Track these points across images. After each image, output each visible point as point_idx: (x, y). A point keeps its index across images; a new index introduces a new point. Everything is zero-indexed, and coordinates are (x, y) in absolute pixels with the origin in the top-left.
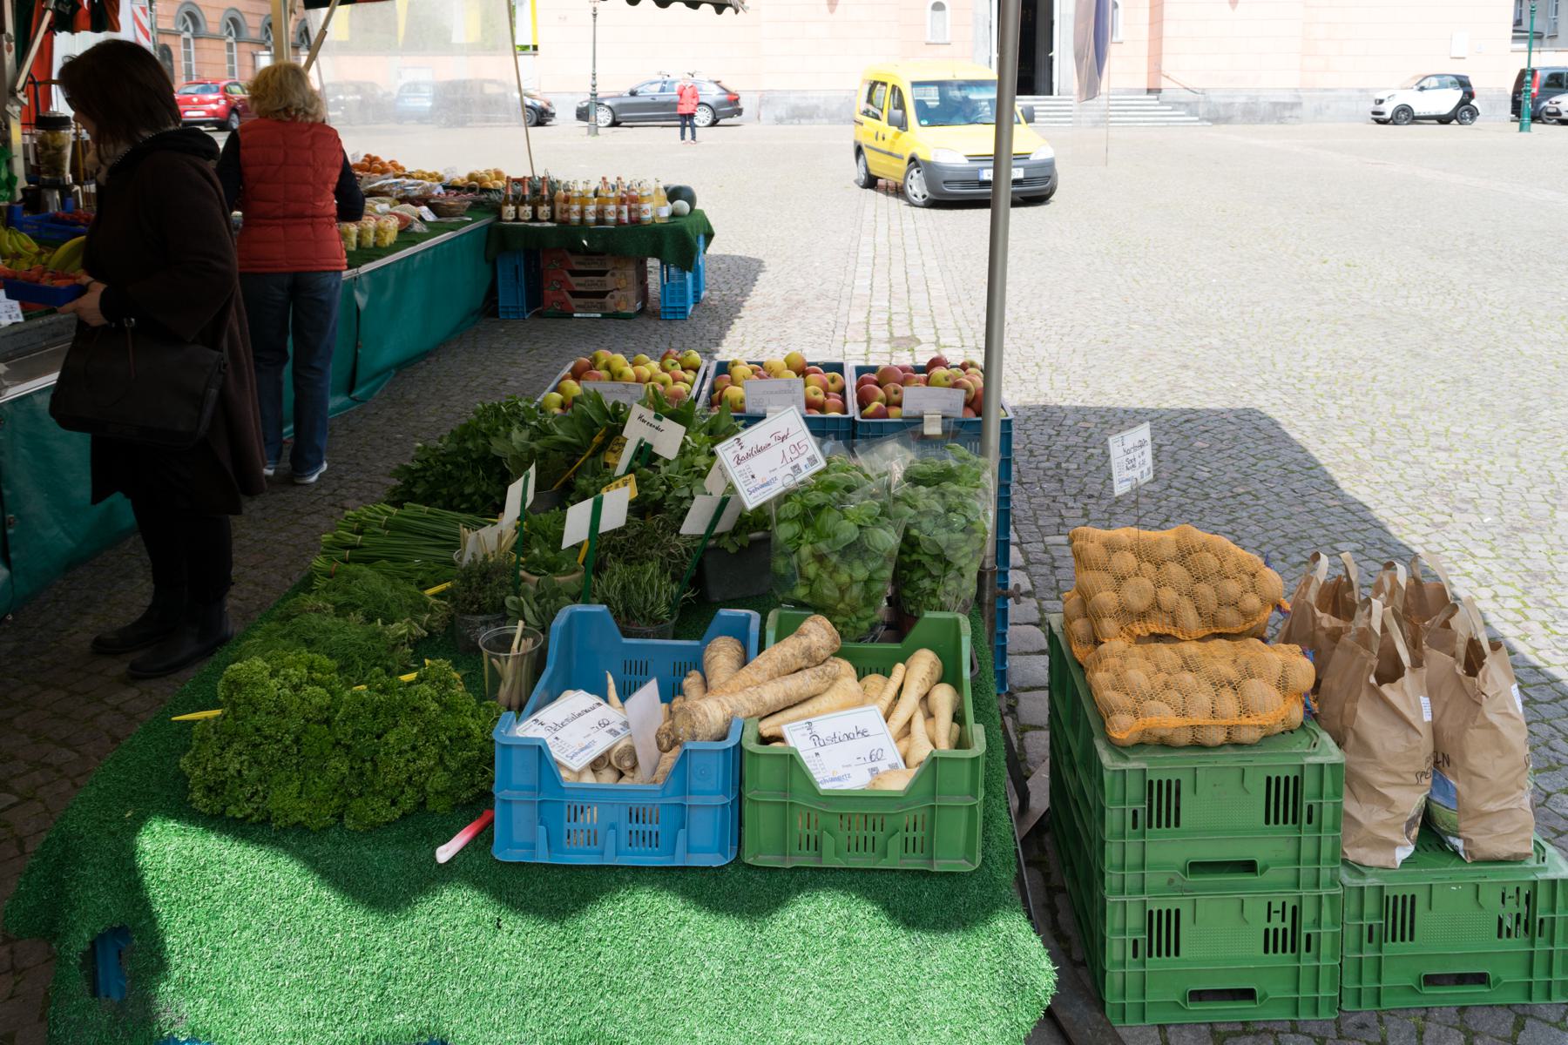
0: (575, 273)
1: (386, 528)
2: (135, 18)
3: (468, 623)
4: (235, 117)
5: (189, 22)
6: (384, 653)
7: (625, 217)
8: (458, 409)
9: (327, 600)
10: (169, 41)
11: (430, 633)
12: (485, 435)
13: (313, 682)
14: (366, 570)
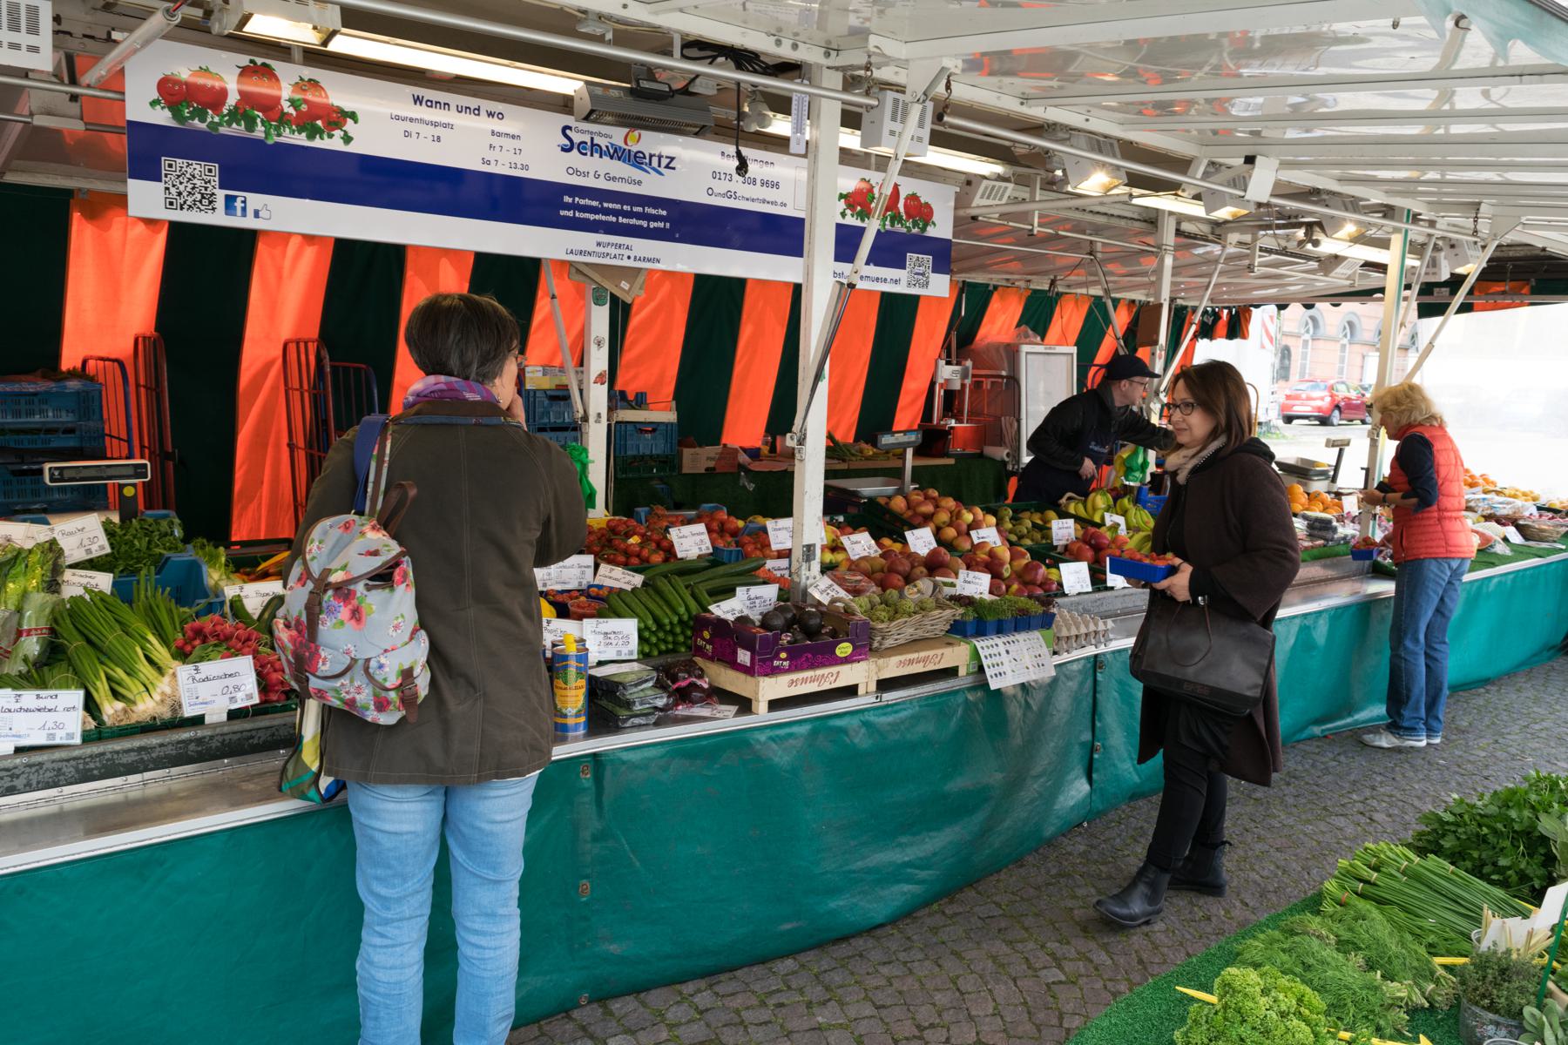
1: (1404, 873)
2: (1264, 325)
3: (1475, 1015)
4: (1336, 413)
5: (1311, 325)
6: (1377, 1009)
8: (1513, 751)
9: (1331, 930)
10: (1290, 342)
11: (1432, 1005)
12: (1533, 807)
13: (1299, 1015)
14: (1375, 913)
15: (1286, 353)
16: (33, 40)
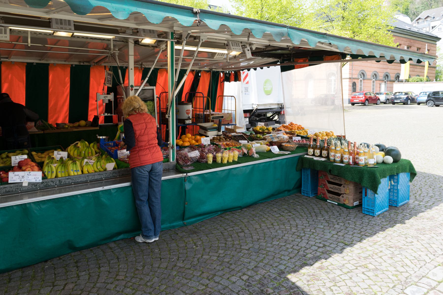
0: (330, 183)
4: (367, 102)
7: (351, 161)
10: (355, 81)
15: (354, 84)
16: (5, 35)
